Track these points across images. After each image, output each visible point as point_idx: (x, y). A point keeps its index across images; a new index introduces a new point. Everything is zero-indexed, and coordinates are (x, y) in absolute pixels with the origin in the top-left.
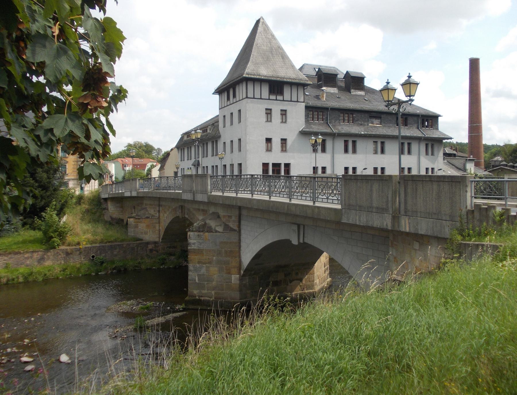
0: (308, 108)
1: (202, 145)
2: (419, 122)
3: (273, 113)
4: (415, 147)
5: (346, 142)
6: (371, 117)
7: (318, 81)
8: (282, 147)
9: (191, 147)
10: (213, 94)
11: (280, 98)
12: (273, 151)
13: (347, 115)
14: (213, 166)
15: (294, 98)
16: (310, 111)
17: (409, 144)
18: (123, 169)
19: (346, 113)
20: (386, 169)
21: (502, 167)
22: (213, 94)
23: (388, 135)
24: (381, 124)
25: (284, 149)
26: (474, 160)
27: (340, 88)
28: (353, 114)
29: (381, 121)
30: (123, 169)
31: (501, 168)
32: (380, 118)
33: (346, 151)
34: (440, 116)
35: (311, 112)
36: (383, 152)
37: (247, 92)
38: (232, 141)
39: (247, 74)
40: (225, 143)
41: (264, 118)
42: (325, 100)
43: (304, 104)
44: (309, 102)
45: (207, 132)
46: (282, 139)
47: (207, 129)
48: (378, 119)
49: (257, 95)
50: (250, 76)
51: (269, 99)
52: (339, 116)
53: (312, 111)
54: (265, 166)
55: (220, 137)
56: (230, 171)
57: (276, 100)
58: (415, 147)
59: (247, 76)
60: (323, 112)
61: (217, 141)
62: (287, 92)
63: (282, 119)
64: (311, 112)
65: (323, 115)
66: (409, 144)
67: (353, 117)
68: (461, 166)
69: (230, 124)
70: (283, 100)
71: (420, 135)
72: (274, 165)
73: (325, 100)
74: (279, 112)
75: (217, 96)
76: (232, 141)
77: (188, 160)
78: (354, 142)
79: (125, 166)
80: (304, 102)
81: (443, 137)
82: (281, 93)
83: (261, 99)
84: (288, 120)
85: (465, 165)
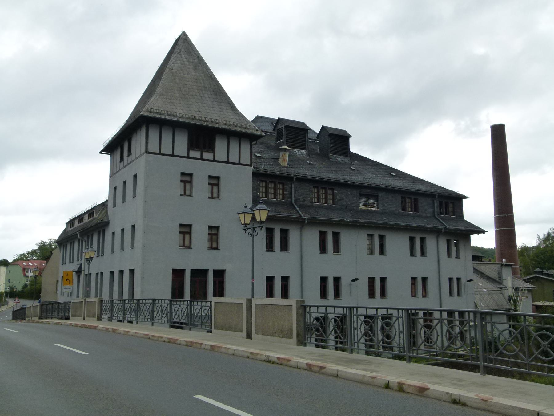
0: (256, 175)
1: (86, 238)
2: (436, 205)
3: (196, 180)
4: (431, 243)
5: (323, 235)
6: (363, 195)
7: (278, 139)
8: (211, 240)
9: (74, 242)
10: (101, 153)
11: (207, 155)
12: (220, 248)
13: (324, 192)
14: (97, 274)
15: (234, 158)
16: (262, 181)
17: (422, 240)
18: (25, 276)
19: (322, 188)
20: (388, 279)
21: (537, 275)
22: (101, 153)
23: (390, 225)
24: (377, 207)
25: (214, 245)
26: (511, 265)
27: (311, 153)
28: (333, 190)
29: (378, 201)
30: (25, 276)
31: (536, 276)
32: (376, 197)
33: (323, 249)
34: (464, 197)
35: (264, 184)
36: (382, 251)
37: (147, 143)
38: (123, 230)
39: (147, 111)
40: (113, 233)
41: (178, 188)
42: (287, 165)
43: (250, 170)
44: (259, 166)
45: (93, 216)
46: (210, 227)
47: (93, 212)
48: (373, 199)
49: (167, 149)
50: (152, 115)
51: (188, 157)
52: (311, 191)
53: (266, 182)
54: (178, 274)
55: (107, 224)
56: (129, 283)
57: (201, 159)
58: (431, 243)
59: (147, 114)
60: (283, 184)
61: (104, 231)
62: (221, 146)
63: (212, 192)
64: (264, 184)
65: (283, 189)
66: (422, 240)
67: (333, 194)
68: (494, 275)
69: (121, 200)
70: (214, 161)
71: (439, 226)
72: (194, 272)
73: (287, 165)
74: (207, 181)
75: (107, 158)
76: (123, 230)
77: (70, 263)
78: (336, 236)
79: (27, 272)
80: (250, 165)
81: (472, 229)
82: (211, 148)
83: (173, 155)
84: (222, 194)
85: (500, 274)
